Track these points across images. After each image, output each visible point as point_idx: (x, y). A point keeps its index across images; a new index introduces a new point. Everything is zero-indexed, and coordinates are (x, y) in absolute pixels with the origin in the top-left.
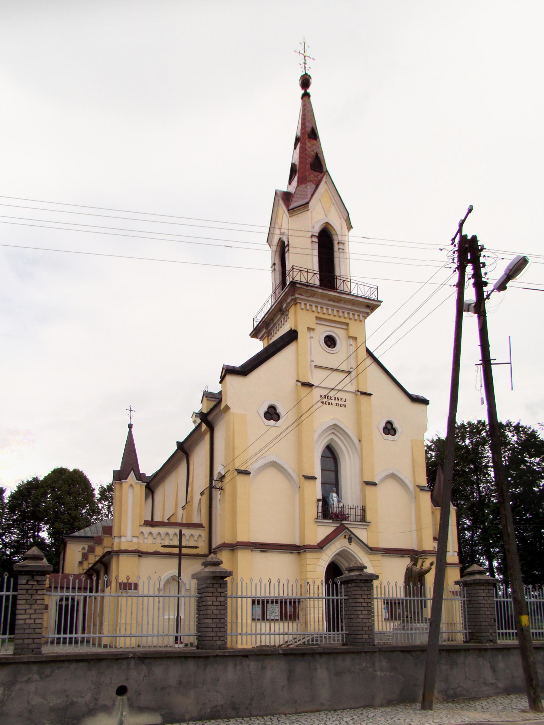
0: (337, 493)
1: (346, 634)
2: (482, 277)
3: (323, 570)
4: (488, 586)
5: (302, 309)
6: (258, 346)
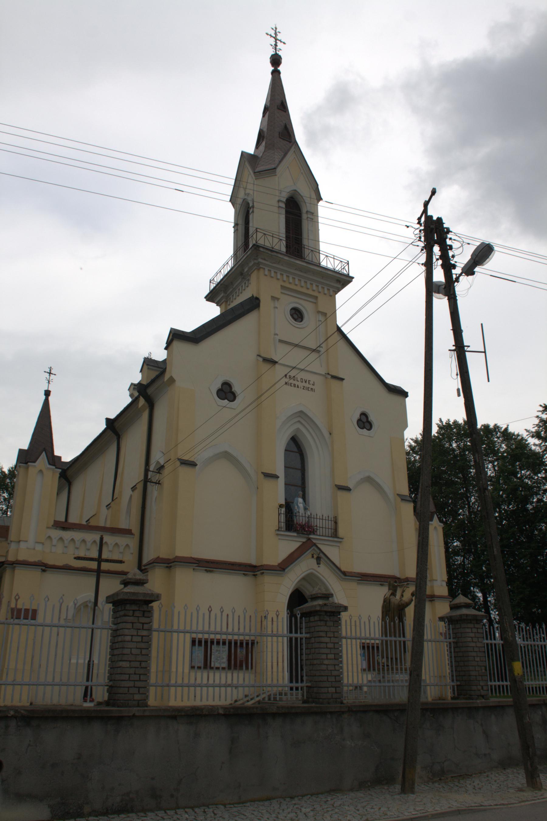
0: (304, 498)
1: (307, 686)
2: (450, 259)
3: (284, 599)
4: (477, 623)
5: (266, 275)
6: (213, 311)
